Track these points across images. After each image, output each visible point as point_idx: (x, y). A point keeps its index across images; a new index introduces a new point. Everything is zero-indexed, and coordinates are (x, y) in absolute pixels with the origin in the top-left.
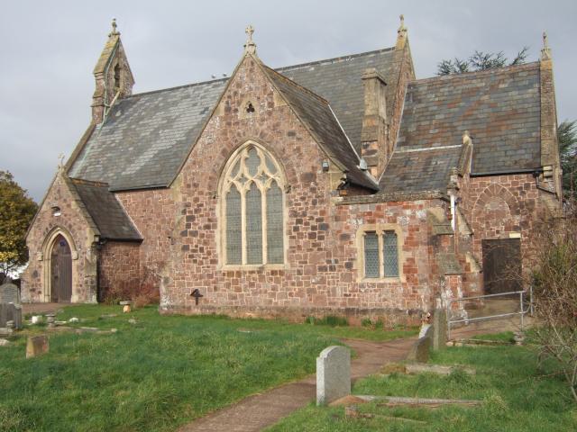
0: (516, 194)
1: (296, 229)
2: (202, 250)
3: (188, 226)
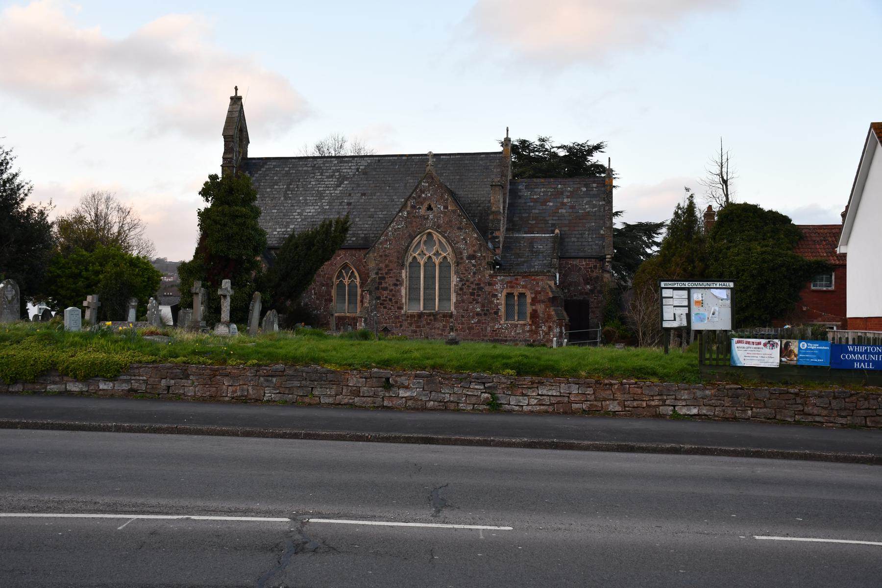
0: (588, 271)
1: (461, 289)
2: (390, 300)
3: (380, 283)
